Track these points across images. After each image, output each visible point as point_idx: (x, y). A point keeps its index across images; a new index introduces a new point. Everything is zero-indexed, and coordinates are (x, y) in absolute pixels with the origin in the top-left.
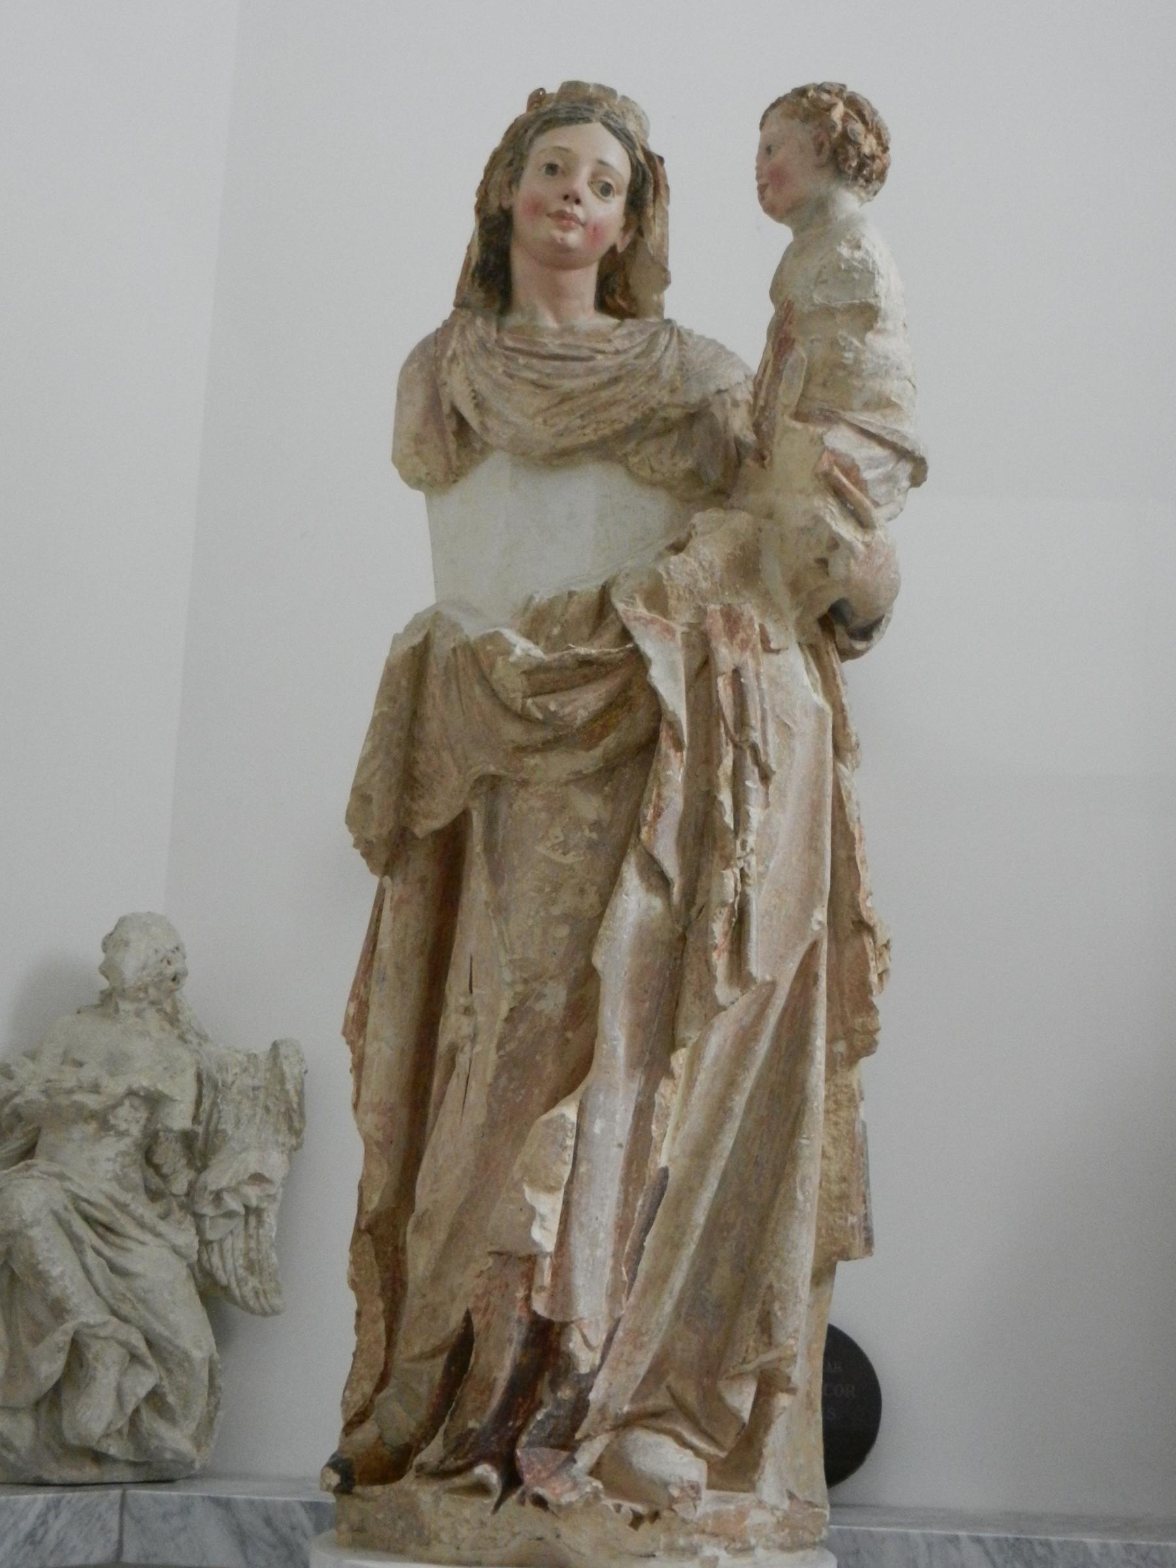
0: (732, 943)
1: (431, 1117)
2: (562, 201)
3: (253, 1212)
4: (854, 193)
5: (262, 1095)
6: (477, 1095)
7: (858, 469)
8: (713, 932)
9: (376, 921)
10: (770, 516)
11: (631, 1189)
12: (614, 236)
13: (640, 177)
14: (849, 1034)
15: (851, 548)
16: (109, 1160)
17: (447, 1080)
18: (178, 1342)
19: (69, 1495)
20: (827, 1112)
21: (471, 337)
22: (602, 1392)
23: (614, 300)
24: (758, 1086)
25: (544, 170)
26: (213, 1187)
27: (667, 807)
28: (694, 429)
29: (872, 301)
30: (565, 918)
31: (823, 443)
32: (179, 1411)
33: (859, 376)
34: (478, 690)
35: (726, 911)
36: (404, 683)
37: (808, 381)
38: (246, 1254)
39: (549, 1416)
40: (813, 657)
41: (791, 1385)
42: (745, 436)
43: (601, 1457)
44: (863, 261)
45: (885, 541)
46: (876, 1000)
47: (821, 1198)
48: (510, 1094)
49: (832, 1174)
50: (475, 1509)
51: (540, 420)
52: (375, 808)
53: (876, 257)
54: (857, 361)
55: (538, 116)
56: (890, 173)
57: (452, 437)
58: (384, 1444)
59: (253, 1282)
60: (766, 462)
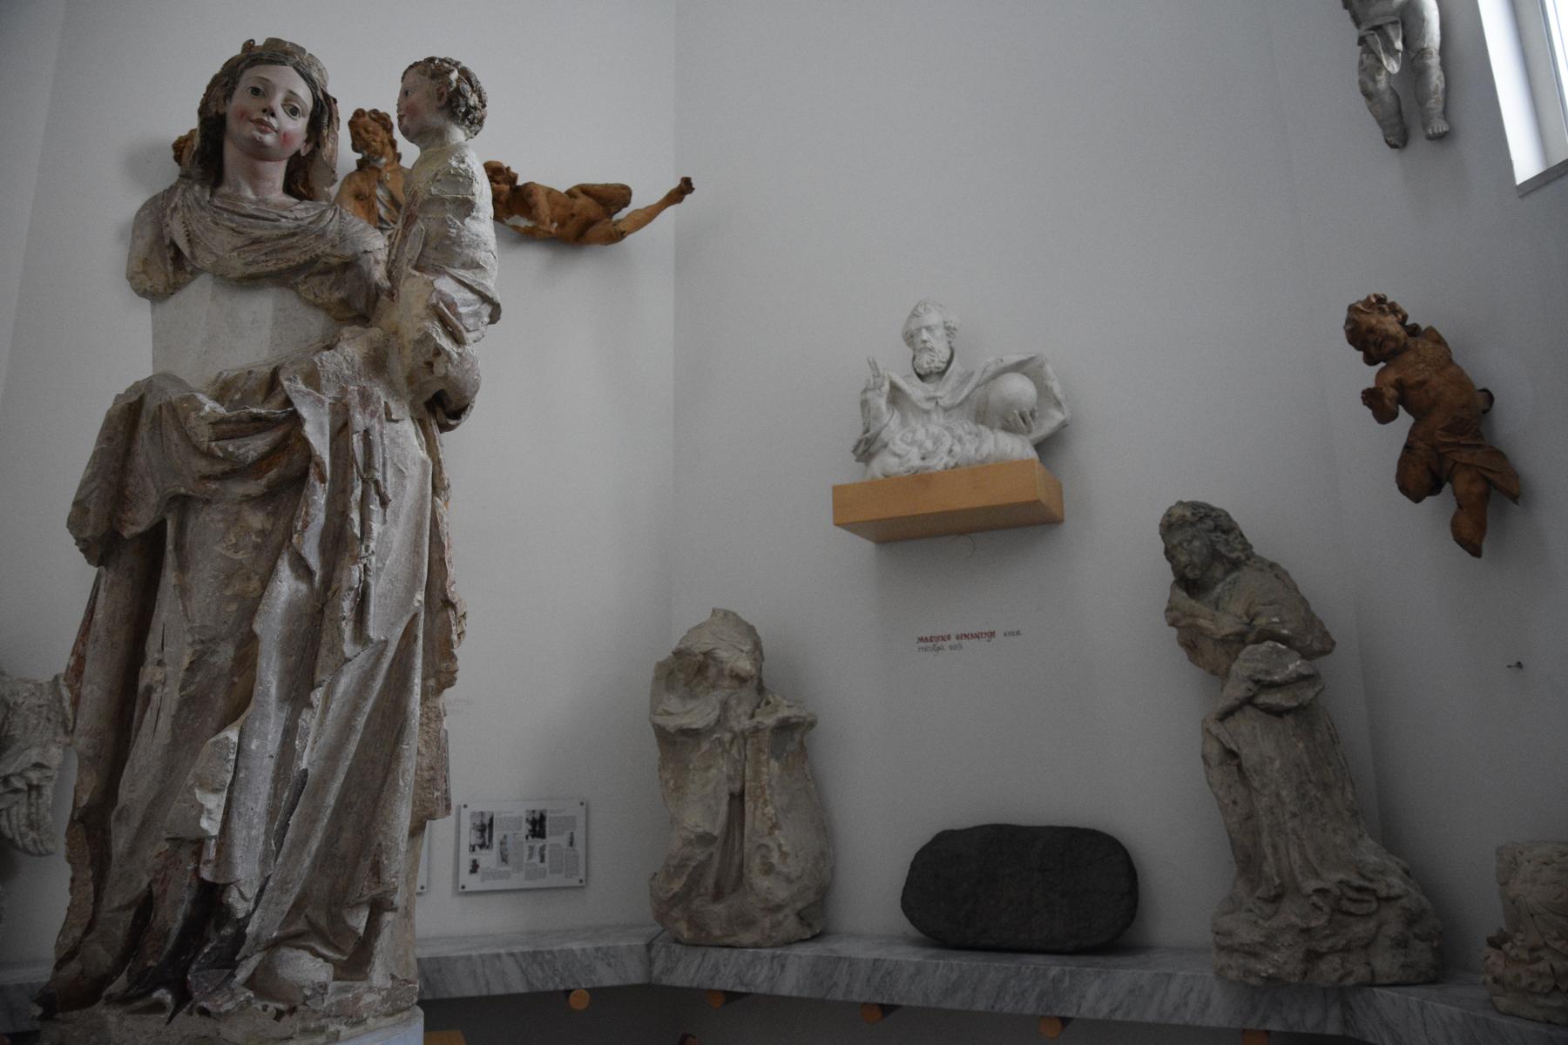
0: (356, 615)
1: (133, 737)
5: (45, 711)
6: (164, 724)
8: (343, 608)
9: (91, 611)
10: (396, 333)
11: (279, 786)
12: (299, 144)
13: (319, 109)
14: (437, 674)
15: (449, 355)
17: (144, 712)
20: (421, 724)
22: (256, 925)
23: (297, 187)
24: (374, 709)
25: (249, 91)
27: (313, 520)
28: (347, 273)
29: (470, 197)
30: (235, 597)
31: (433, 286)
33: (460, 246)
34: (175, 436)
36: (121, 428)
37: (425, 245)
38: (28, 816)
39: (213, 949)
40: (422, 429)
41: (394, 906)
42: (382, 283)
43: (256, 969)
46: (456, 651)
47: (416, 781)
48: (190, 722)
49: (424, 765)
50: (155, 1022)
52: (91, 517)
53: (475, 169)
54: (459, 236)
56: (486, 121)
57: (169, 261)
59: (32, 835)
60: (395, 297)
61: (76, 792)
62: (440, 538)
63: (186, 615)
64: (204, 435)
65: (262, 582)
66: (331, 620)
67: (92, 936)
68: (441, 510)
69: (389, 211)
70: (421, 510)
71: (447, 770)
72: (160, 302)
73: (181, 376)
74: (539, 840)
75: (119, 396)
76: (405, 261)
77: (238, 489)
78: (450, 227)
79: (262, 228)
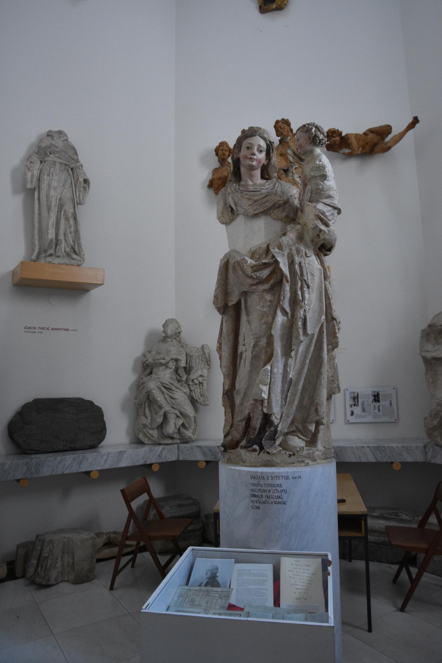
0: (303, 327)
1: (238, 368)
2: (251, 155)
3: (201, 383)
4: (319, 148)
5: (201, 357)
6: (248, 364)
7: (325, 213)
8: (299, 324)
9: (221, 329)
11: (284, 383)
12: (264, 162)
15: (324, 232)
16: (168, 374)
17: (241, 360)
18: (187, 413)
19: (166, 447)
20: (328, 361)
21: (232, 188)
24: (312, 357)
25: (246, 148)
26: (192, 379)
27: (286, 296)
29: (325, 173)
31: (316, 208)
32: (188, 427)
33: (323, 191)
34: (240, 272)
35: (301, 319)
36: (224, 271)
37: (312, 193)
38: (200, 393)
39: (269, 434)
40: (318, 257)
43: (281, 442)
44: (322, 164)
45: (332, 229)
46: (338, 335)
47: (328, 381)
48: (255, 363)
51: (250, 207)
52: (219, 300)
54: (323, 187)
55: (244, 136)
58: (233, 441)
59: (202, 399)
60: (303, 212)
61: (223, 385)
62: (328, 296)
63: (251, 329)
64: (249, 271)
65: (272, 317)
66: (295, 328)
67: (233, 429)
68: (328, 286)
69: (293, 158)
70: (321, 287)
71: (338, 377)
72: (228, 225)
73: (238, 250)
74: (377, 403)
75: (221, 260)
76: (305, 200)
77: (262, 287)
78: (319, 185)
79: (257, 196)
